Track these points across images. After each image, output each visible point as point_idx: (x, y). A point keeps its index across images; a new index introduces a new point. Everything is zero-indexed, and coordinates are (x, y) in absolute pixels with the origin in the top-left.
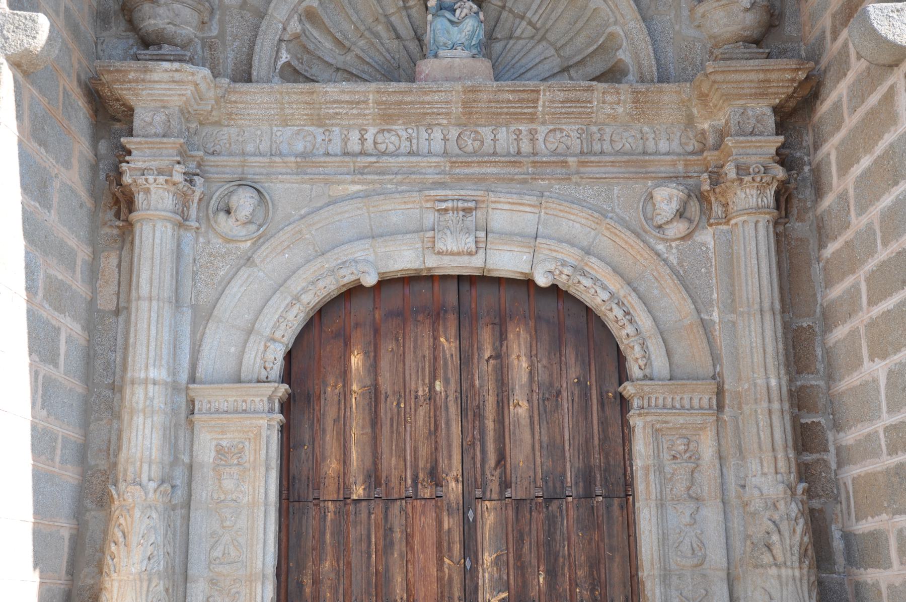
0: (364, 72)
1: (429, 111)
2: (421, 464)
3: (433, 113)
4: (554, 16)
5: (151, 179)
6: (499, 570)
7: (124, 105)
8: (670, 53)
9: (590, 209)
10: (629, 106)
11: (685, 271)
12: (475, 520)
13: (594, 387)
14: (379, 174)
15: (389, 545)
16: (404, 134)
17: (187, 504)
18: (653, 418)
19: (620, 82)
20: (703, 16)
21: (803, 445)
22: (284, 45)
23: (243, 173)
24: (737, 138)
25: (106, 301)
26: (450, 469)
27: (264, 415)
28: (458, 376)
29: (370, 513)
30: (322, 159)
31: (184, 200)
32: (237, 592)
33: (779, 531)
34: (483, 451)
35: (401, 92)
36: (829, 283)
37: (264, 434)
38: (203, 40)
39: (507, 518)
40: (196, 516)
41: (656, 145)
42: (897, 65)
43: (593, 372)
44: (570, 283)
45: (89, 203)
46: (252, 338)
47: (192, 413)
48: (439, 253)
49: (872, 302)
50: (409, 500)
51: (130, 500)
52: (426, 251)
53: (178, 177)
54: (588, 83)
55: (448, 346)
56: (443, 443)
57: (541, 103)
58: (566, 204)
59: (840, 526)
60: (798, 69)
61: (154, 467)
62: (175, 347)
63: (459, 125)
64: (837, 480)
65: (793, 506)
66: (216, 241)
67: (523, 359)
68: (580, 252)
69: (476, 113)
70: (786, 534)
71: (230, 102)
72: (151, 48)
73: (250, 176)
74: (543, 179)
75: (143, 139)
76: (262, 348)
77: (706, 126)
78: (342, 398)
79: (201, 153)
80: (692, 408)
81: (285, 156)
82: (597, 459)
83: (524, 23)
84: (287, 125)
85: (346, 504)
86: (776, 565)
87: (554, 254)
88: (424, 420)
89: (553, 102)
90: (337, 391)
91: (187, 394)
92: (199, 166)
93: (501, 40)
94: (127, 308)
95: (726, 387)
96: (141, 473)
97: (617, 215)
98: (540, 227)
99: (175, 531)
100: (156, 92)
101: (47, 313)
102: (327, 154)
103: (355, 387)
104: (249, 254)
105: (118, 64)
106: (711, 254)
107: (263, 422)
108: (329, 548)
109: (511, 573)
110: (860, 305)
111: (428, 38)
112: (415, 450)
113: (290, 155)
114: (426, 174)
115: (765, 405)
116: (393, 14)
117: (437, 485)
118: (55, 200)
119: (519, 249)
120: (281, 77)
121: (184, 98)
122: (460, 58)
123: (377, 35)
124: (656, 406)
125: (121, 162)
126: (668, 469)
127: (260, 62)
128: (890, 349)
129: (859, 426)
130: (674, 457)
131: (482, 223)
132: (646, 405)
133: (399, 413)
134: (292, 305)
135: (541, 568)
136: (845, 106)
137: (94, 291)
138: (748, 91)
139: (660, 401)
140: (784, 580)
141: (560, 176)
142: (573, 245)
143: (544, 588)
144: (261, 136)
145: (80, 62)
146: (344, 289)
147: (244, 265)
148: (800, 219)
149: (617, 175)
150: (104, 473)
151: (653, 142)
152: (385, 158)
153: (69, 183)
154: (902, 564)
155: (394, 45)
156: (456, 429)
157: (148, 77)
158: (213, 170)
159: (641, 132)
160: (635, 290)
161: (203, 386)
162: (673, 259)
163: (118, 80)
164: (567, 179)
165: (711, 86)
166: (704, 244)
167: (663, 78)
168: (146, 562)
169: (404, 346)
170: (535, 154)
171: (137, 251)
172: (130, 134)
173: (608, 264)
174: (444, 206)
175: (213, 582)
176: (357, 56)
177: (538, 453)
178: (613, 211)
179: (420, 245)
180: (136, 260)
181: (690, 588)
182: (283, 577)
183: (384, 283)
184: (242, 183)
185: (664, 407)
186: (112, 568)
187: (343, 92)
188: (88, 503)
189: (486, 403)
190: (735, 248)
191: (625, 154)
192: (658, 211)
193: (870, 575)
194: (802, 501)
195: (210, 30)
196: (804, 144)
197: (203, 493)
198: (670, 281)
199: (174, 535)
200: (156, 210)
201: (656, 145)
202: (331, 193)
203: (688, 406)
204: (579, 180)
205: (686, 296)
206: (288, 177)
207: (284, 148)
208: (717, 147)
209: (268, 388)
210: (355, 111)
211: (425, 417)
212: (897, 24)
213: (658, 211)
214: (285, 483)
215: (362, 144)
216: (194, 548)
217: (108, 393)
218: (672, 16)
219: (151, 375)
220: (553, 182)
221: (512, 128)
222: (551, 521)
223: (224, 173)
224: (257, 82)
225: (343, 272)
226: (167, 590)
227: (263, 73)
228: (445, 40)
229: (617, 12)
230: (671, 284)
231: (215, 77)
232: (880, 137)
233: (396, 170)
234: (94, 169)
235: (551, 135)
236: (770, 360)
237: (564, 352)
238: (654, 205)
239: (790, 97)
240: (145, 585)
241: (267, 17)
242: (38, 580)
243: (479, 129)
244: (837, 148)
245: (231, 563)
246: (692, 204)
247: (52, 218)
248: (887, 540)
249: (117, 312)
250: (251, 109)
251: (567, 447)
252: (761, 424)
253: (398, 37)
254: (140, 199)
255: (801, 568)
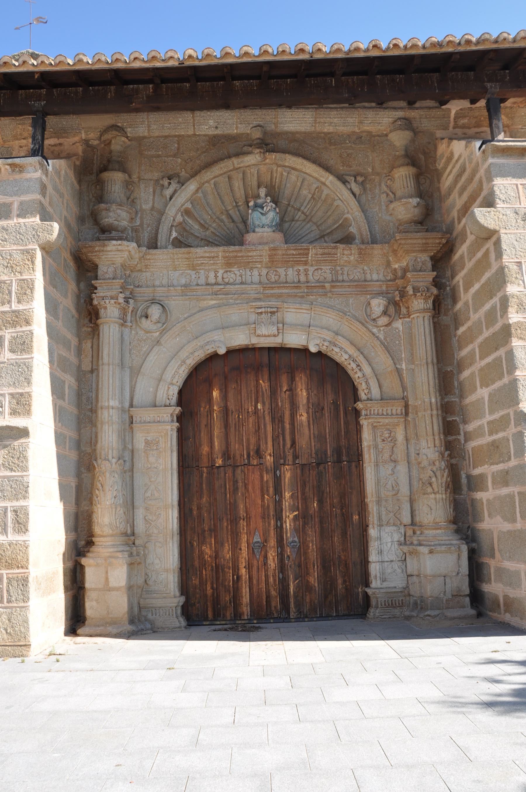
0: (216, 240)
1: (251, 260)
2: (252, 447)
3: (253, 262)
4: (315, 209)
5: (107, 301)
6: (293, 501)
7: (93, 263)
8: (377, 228)
9: (337, 311)
10: (356, 256)
11: (388, 343)
12: (280, 475)
13: (341, 405)
14: (226, 294)
15: (236, 490)
16: (238, 273)
17: (132, 470)
18: (373, 420)
19: (351, 244)
20: (393, 209)
21: (448, 432)
22: (174, 228)
23: (154, 296)
24: (413, 273)
25: (86, 366)
26: (267, 449)
27: (169, 424)
28: (270, 401)
29: (225, 473)
30: (195, 288)
31: (124, 312)
32: (159, 514)
33: (436, 476)
34: (284, 440)
35: (236, 251)
36: (460, 348)
37: (169, 434)
38: (132, 227)
39: (297, 474)
40: (137, 476)
41: (371, 276)
42: (489, 239)
43: (341, 397)
44: (328, 350)
45: (76, 316)
46: (161, 383)
47: (132, 423)
48: (258, 336)
49: (481, 358)
50: (246, 466)
51: (104, 468)
52: (251, 335)
53: (121, 300)
54: (334, 244)
55: (264, 384)
56: (262, 435)
57: (310, 255)
58: (324, 308)
59: (465, 471)
60: (443, 238)
61: (114, 451)
62: (122, 389)
63: (267, 268)
64: (465, 448)
65: (443, 463)
66: (141, 333)
67: (304, 391)
68: (333, 334)
69: (276, 261)
70: (439, 477)
71: (147, 259)
72: (106, 233)
73: (157, 298)
74: (312, 295)
75: (103, 281)
76: (166, 388)
77: (396, 266)
78: (209, 414)
79: (132, 287)
80: (392, 414)
81: (176, 286)
82: (343, 442)
83: (300, 213)
84: (176, 270)
85: (213, 469)
86: (434, 493)
87: (319, 335)
88: (252, 424)
89: (317, 254)
90: (206, 410)
91: (129, 413)
92: (131, 293)
93: (288, 222)
94: (97, 369)
95: (410, 403)
96: (108, 455)
97: (352, 314)
98: (311, 321)
99: (126, 484)
100: (109, 256)
101: (59, 374)
102: (198, 285)
103: (215, 408)
104: (158, 339)
105: (90, 243)
106: (401, 334)
107: (169, 427)
108: (205, 491)
109: (300, 502)
110: (476, 359)
111: (250, 221)
112: (248, 440)
113: (178, 286)
114: (250, 294)
115: (429, 412)
116: (230, 209)
117: (260, 458)
118: (61, 315)
119: (301, 333)
120: (173, 245)
121: (123, 259)
122: (267, 232)
123: (222, 221)
124: (374, 414)
125: (92, 293)
126: (380, 447)
127: (161, 238)
128: (490, 382)
129: (475, 421)
130: (383, 440)
131: (280, 319)
132: (368, 414)
133: (239, 421)
134: (182, 365)
135: (315, 499)
136: (466, 257)
137: (80, 361)
138: (417, 249)
139: (376, 412)
140: (438, 500)
141: (321, 294)
142: (329, 330)
143: (317, 510)
144: (163, 276)
145: (71, 243)
146: (208, 356)
147: (156, 345)
148: (446, 315)
149: (351, 293)
150: (89, 454)
151: (369, 275)
152: (228, 286)
153: (67, 306)
154: (493, 489)
155: (232, 225)
156: (269, 428)
157: (105, 249)
158: (138, 295)
159: (363, 270)
160: (362, 353)
161: (137, 409)
162: (382, 337)
163: (90, 251)
164: (325, 295)
165: (399, 246)
166: (397, 328)
167: (374, 241)
168: (113, 499)
169: (241, 386)
170: (308, 282)
171: (101, 339)
172: (96, 278)
173: (348, 340)
174: (260, 310)
175: (147, 509)
176: (212, 232)
177: (312, 440)
178: (349, 312)
179: (247, 332)
180: (101, 344)
181: (391, 506)
182: (182, 506)
183: (230, 352)
184: (153, 301)
185: (378, 414)
186: (97, 502)
187: (205, 252)
188: (83, 469)
189: (285, 415)
190: (413, 330)
191: (355, 281)
192: (373, 311)
193: (479, 495)
194: (447, 461)
195: (136, 222)
196: (447, 276)
197: (139, 464)
198: (380, 348)
199: (126, 485)
200: (110, 318)
201: (371, 276)
202: (200, 305)
203: (390, 414)
204: (331, 295)
205: (388, 356)
206: (177, 297)
207: (175, 282)
208: (403, 277)
209: (170, 410)
210: (212, 262)
211: (253, 422)
212: (489, 219)
213: (373, 311)
214: (181, 458)
215: (216, 279)
216: (136, 492)
217: (89, 413)
218: (377, 209)
219: (111, 404)
220: (318, 297)
221: (295, 269)
222: (320, 475)
223: (144, 297)
224: (161, 248)
225: (207, 347)
226: (125, 513)
227: (163, 243)
228: (259, 223)
229: (348, 207)
230: (381, 350)
231: (139, 247)
232: (483, 274)
233: (234, 292)
234: (78, 297)
235: (316, 272)
236: (432, 389)
237: (325, 387)
238: (371, 308)
239: (438, 252)
240: (114, 510)
241: (165, 214)
242: (63, 507)
243: (278, 269)
244: (463, 279)
245: (156, 499)
246: (391, 307)
247: (59, 324)
248: (487, 477)
249: (92, 371)
250: (158, 262)
251: (328, 437)
252: (427, 422)
253: (233, 221)
254: (102, 312)
255: (446, 494)
